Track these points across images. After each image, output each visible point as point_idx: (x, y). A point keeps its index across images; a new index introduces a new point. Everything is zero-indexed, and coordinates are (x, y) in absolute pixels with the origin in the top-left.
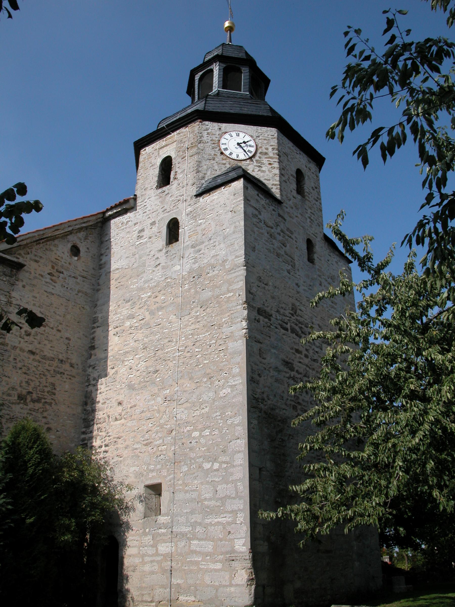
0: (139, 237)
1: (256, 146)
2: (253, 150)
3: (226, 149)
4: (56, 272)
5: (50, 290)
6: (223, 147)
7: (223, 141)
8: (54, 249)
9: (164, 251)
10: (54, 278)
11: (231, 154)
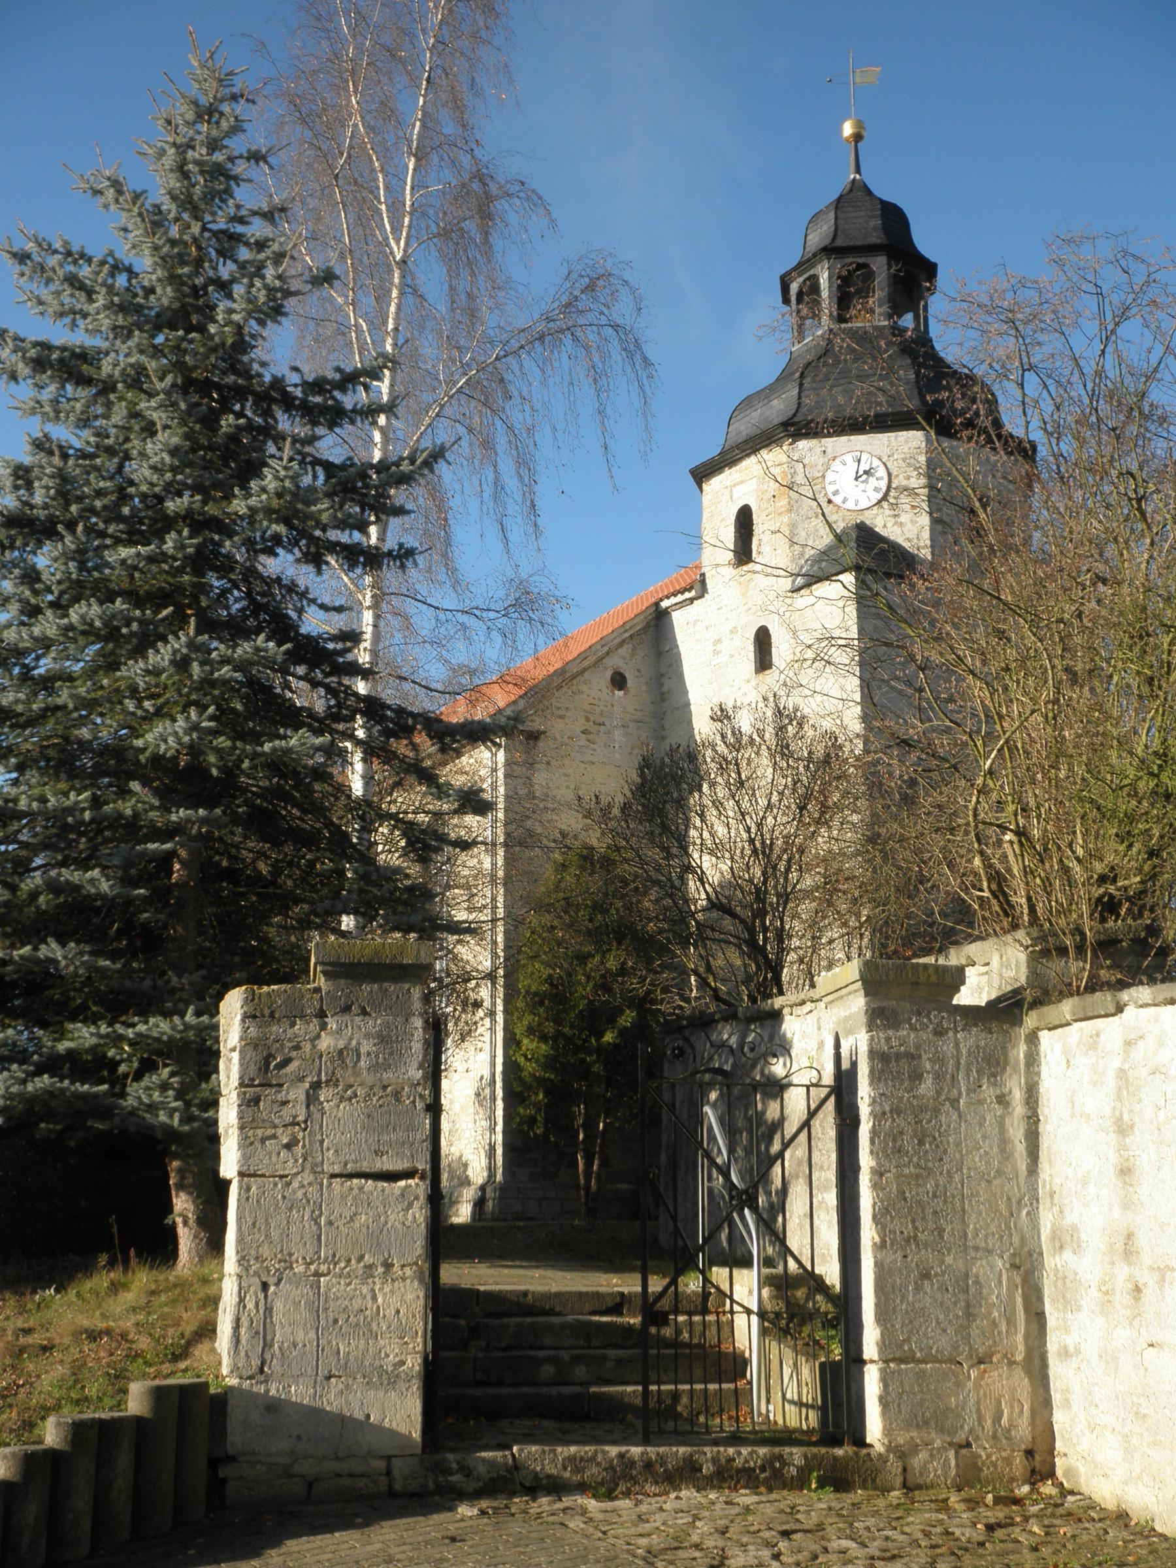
0: (716, 653)
1: (890, 475)
2: (883, 485)
3: (836, 493)
4: (595, 725)
5: (588, 758)
6: (830, 489)
7: (830, 476)
8: (584, 688)
9: (753, 683)
10: (591, 737)
11: (845, 500)
